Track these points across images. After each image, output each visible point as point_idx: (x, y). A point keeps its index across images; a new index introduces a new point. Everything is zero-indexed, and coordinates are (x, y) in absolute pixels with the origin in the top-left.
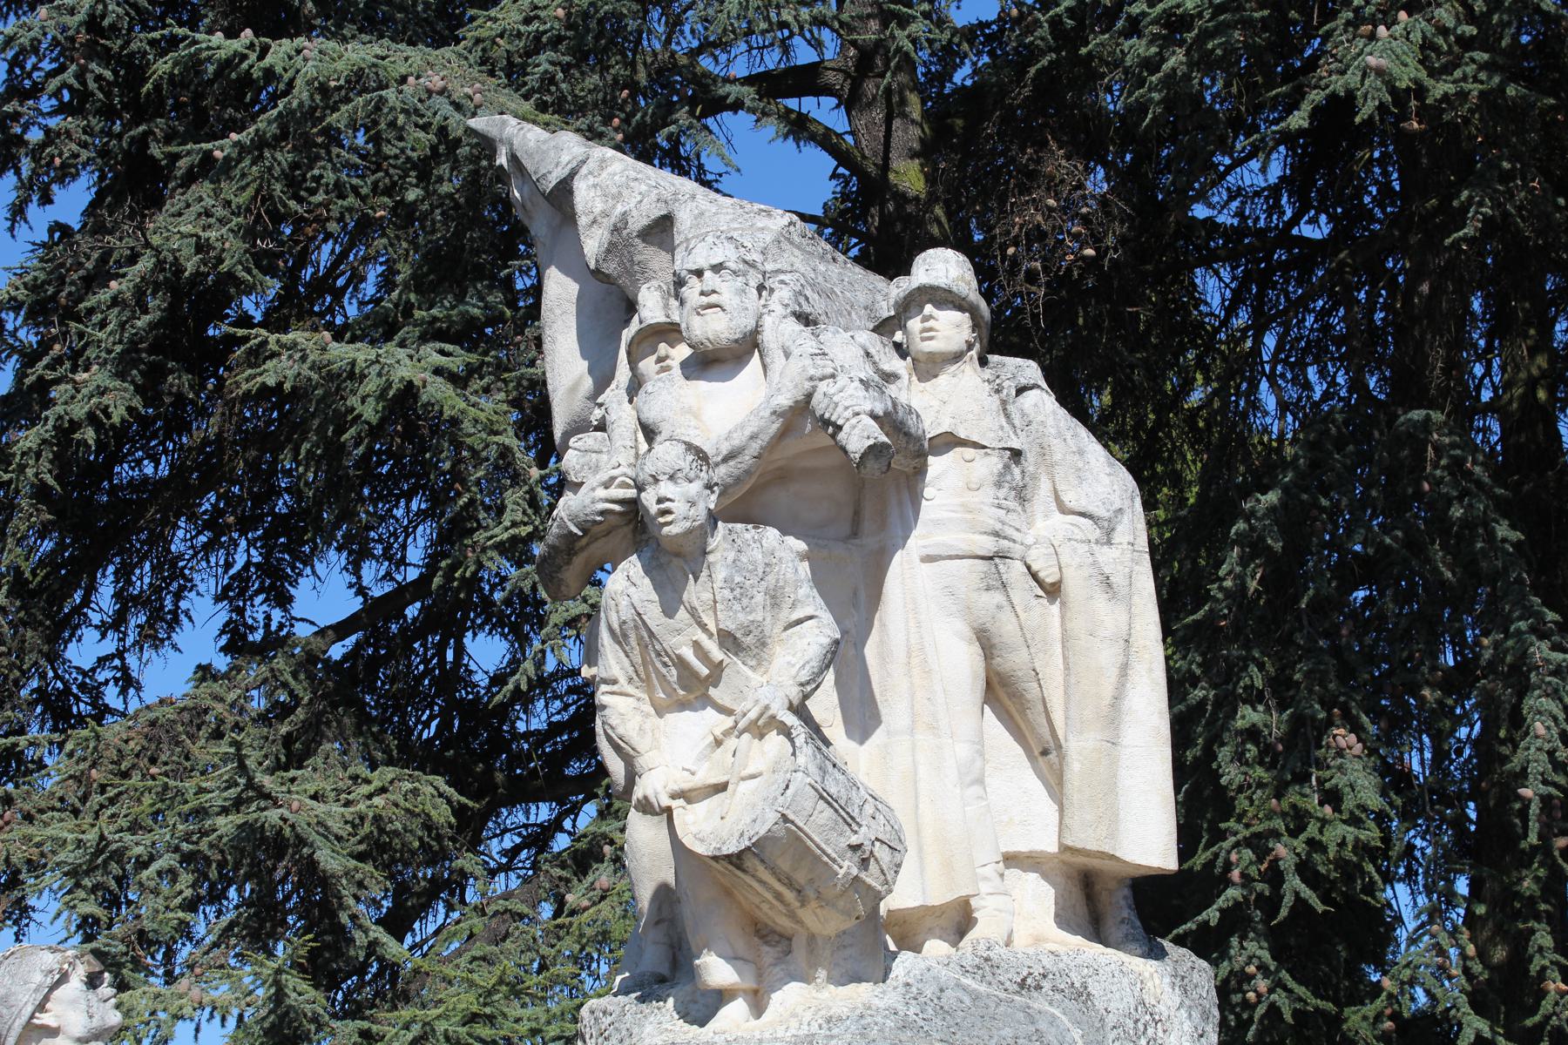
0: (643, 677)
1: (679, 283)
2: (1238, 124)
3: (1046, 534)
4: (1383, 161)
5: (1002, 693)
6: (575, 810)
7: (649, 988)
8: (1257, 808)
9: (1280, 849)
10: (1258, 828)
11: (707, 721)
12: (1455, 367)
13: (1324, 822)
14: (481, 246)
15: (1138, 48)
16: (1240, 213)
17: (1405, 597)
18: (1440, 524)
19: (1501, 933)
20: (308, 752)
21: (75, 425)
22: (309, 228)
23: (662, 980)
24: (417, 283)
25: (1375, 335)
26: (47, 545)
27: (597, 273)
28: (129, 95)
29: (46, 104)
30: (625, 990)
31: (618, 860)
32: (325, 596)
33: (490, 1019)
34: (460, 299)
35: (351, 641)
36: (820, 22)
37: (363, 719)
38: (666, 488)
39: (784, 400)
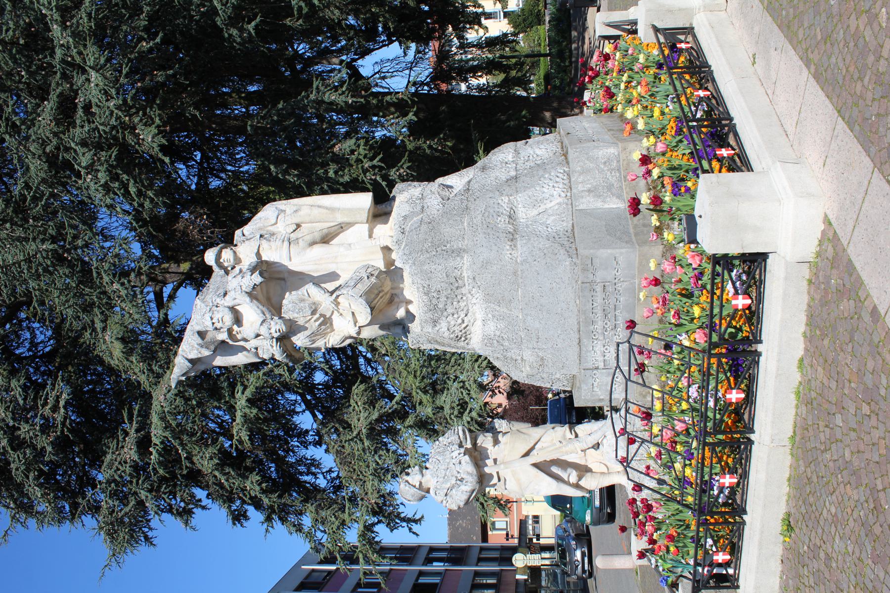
0: (324, 335)
1: (216, 329)
2: (169, 176)
3: (283, 228)
4: (179, 137)
5: (326, 239)
6: (360, 352)
7: (406, 331)
8: (356, 172)
9: (366, 166)
10: (361, 171)
11: (336, 318)
12: (236, 118)
13: (359, 154)
14: (208, 384)
15: (147, 204)
16: (194, 176)
17: (299, 132)
18: (278, 122)
19: (387, 108)
20: (347, 422)
21: (262, 489)
22: (205, 430)
23: (404, 328)
24: (219, 400)
25: (227, 139)
26: (294, 494)
27: (214, 351)
28: (170, 480)
29: (173, 502)
30: (407, 337)
31: (373, 340)
32: (305, 421)
33: (415, 372)
34: (223, 388)
35: (317, 413)
36: (142, 292)
38: (273, 331)
39: (248, 299)
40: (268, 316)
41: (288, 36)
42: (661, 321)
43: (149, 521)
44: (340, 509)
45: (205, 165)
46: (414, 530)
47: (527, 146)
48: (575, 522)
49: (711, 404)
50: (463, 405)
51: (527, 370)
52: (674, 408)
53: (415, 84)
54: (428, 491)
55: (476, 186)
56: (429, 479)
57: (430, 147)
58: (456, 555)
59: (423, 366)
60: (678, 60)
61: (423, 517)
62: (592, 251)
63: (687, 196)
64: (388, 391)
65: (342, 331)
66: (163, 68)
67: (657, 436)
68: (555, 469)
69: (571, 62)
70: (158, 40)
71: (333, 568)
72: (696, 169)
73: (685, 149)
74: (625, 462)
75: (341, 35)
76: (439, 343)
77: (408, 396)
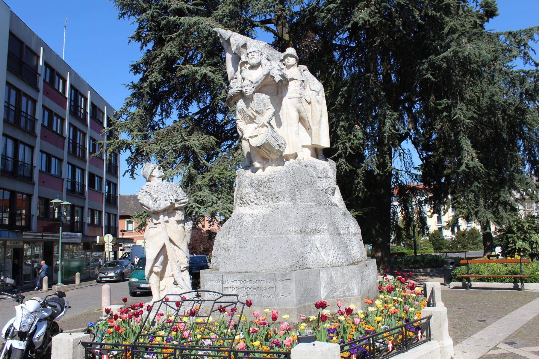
0: (244, 118)
1: (248, 54)
2: (340, 28)
3: (308, 94)
4: (364, 33)
5: (301, 120)
6: (235, 142)
7: (246, 168)
8: (343, 138)
9: (347, 144)
11: (254, 125)
12: (375, 67)
13: (354, 140)
14: (216, 50)
15: (323, 15)
16: (341, 42)
18: (373, 92)
20: (192, 133)
21: (152, 82)
22: (189, 49)
23: (248, 167)
24: (206, 57)
25: (362, 62)
26: (149, 102)
27: (234, 53)
29: (145, 30)
32: (194, 108)
33: (223, 174)
34: (213, 59)
35: (198, 116)
37: (201, 128)
38: (246, 88)
39: (265, 73)
40: (255, 85)
41: (424, 98)
42: (252, 322)
43: (134, 15)
44: (140, 129)
45: (347, 49)
46: (127, 173)
47: (358, 240)
48: (131, 272)
49: (200, 353)
50: (202, 203)
51: (223, 241)
52: (198, 330)
53: (397, 173)
54: (149, 181)
55: (334, 210)
56: (156, 182)
57: (359, 183)
58: (112, 200)
59: (226, 179)
60: (411, 331)
61: (135, 179)
62: (294, 279)
63: (328, 337)
64: (211, 158)
65: (246, 129)
66: (404, 24)
67: (181, 320)
68: (162, 258)
69: (411, 268)
70: (420, 21)
71: (105, 126)
72: (344, 343)
73: (356, 336)
74: (165, 301)
75: (426, 129)
76: (239, 188)
77: (208, 170)
